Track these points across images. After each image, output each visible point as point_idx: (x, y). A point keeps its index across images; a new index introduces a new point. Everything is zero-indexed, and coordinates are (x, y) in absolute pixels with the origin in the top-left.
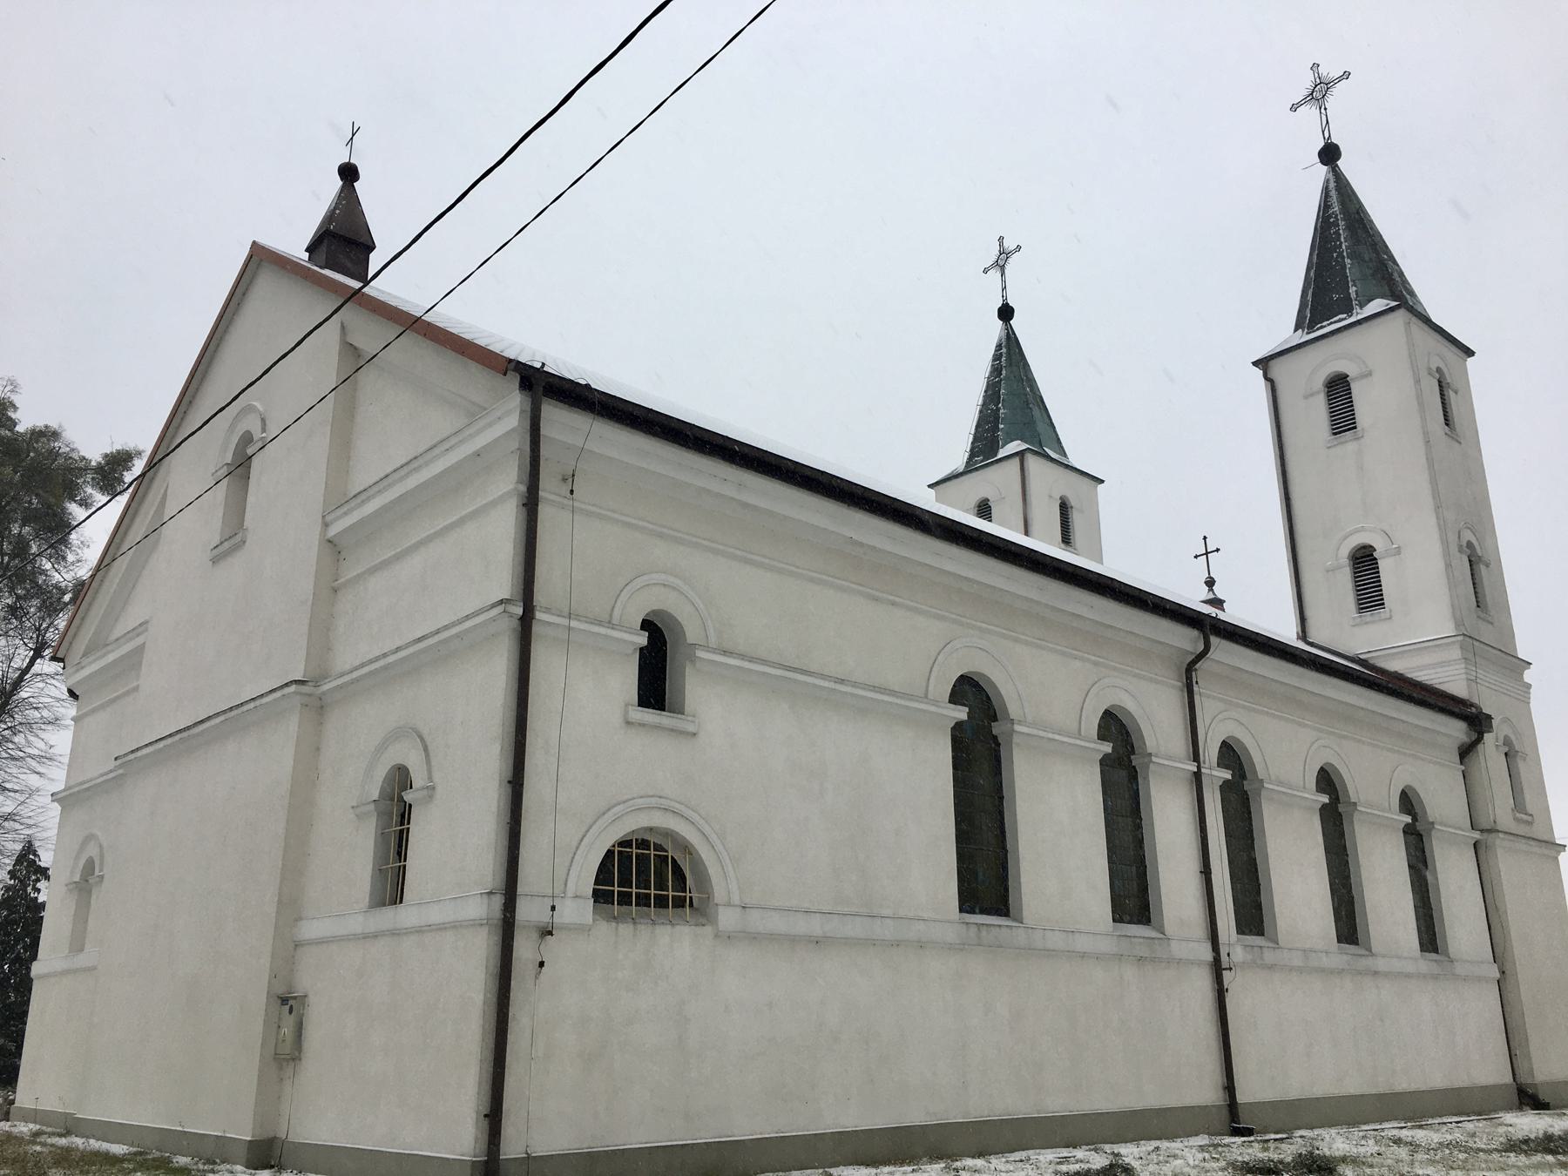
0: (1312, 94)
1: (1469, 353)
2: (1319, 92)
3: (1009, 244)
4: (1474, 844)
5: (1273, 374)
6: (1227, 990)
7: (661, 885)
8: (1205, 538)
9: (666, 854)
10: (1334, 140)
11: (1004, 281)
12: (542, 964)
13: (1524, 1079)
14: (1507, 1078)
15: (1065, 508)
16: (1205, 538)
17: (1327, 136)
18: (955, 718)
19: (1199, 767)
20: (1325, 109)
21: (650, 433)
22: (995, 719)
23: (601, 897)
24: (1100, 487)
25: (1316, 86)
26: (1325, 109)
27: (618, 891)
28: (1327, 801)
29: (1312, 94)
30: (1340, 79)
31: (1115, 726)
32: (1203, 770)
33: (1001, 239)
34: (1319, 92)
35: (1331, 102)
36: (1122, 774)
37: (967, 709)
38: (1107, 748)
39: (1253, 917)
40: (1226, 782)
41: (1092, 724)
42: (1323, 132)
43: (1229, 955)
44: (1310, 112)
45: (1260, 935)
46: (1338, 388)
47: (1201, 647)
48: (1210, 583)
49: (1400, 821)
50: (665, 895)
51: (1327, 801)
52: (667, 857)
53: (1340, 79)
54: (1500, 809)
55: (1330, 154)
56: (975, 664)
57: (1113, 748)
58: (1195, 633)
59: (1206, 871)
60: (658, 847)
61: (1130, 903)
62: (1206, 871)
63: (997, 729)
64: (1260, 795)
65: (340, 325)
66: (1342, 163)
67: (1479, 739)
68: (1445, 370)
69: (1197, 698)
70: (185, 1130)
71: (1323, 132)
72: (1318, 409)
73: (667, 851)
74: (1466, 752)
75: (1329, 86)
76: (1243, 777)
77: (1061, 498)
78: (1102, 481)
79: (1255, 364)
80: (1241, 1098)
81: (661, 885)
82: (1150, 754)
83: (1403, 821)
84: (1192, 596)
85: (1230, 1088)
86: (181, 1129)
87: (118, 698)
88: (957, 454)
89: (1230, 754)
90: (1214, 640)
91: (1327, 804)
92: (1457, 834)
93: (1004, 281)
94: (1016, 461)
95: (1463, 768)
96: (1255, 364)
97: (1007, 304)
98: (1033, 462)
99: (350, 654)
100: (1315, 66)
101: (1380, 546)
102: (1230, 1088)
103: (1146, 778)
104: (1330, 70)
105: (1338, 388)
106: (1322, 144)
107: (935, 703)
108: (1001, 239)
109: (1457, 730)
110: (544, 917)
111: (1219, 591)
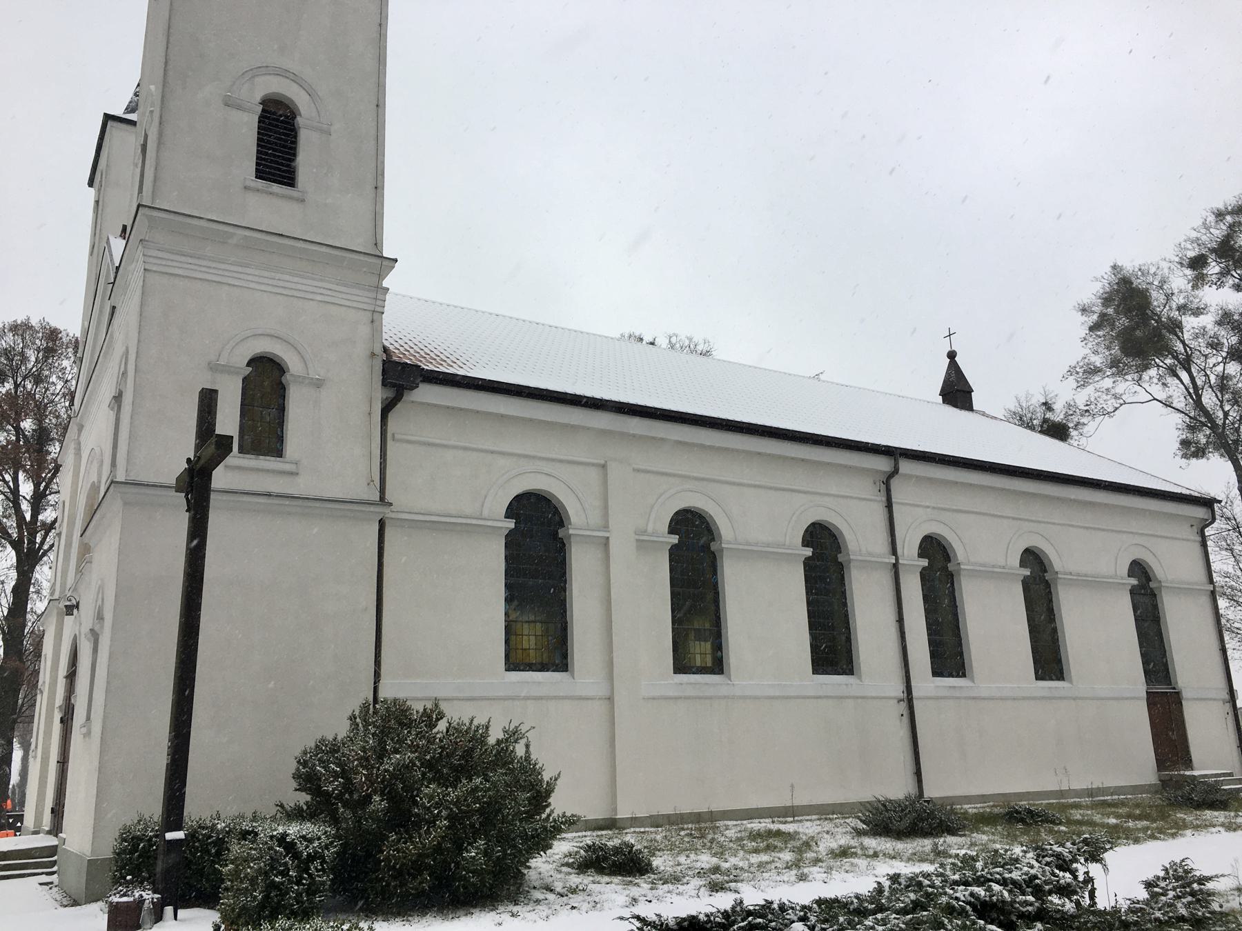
4: (380, 521)
5: (367, 313)
18: (1022, 575)
19: (897, 559)
21: (1120, 492)
22: (1046, 571)
28: (1029, 574)
37: (677, 537)
38: (1134, 581)
40: (924, 569)
41: (1124, 569)
45: (961, 677)
49: (799, 555)
50: (1166, 769)
51: (1029, 574)
55: (952, 355)
56: (1139, 554)
57: (812, 552)
63: (1048, 576)
64: (959, 575)
65: (124, 348)
76: (1149, 579)
82: (1057, 572)
83: (1129, 584)
89: (934, 548)
91: (1028, 576)
92: (1088, 580)
103: (849, 568)
107: (1122, 578)
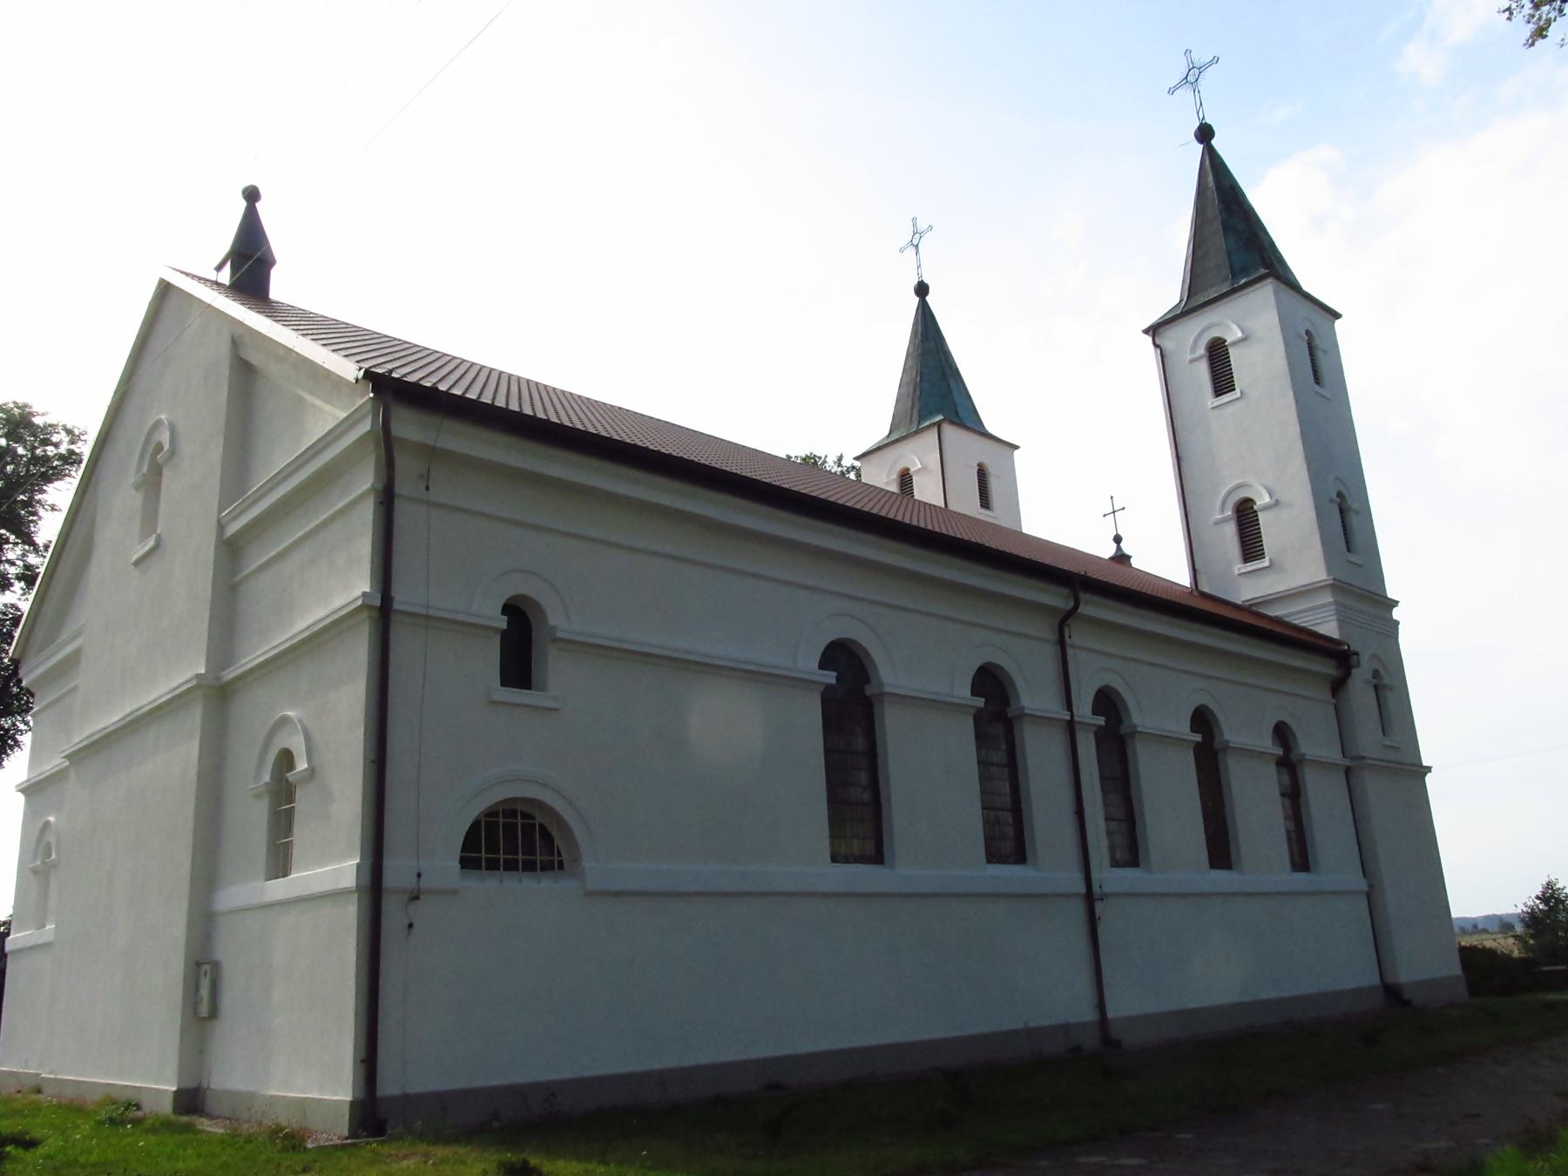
0: (1186, 78)
1: (1337, 316)
2: (1192, 77)
3: (922, 226)
6: (1099, 918)
7: (530, 850)
8: (1112, 498)
9: (533, 822)
10: (1208, 121)
11: (919, 260)
12: (411, 926)
13: (1390, 980)
14: (1376, 981)
15: (982, 474)
16: (1112, 498)
17: (1201, 118)
20: (1199, 92)
23: (468, 863)
24: (1016, 453)
25: (1190, 70)
26: (1199, 92)
27: (504, 859)
29: (1186, 78)
30: (1210, 64)
31: (990, 682)
32: (1076, 719)
33: (914, 219)
34: (1192, 77)
35: (1203, 84)
36: (999, 729)
39: (1130, 852)
42: (1198, 113)
43: (1101, 887)
44: (1185, 94)
46: (1217, 354)
47: (1072, 604)
48: (1118, 539)
52: (535, 824)
53: (1210, 64)
54: (1369, 741)
58: (1066, 591)
59: (1080, 812)
60: (525, 815)
61: (1007, 847)
62: (1080, 812)
66: (1214, 142)
67: (1348, 674)
68: (1314, 332)
69: (1070, 652)
70: (59, 1077)
71: (1198, 113)
72: (1203, 370)
73: (534, 818)
74: (1338, 686)
75: (1201, 70)
77: (979, 465)
78: (1017, 447)
79: (1146, 332)
80: (1110, 1014)
81: (530, 850)
84: (358, 653)
85: (1101, 1006)
86: (52, 1076)
87: (975, 625)
88: (878, 427)
89: (1107, 701)
90: (1083, 596)
93: (919, 260)
94: (935, 430)
95: (1334, 701)
96: (1146, 332)
97: (922, 281)
98: (950, 431)
99: (253, 655)
100: (1188, 52)
101: (1262, 499)
102: (1101, 1006)
104: (1201, 57)
105: (1217, 354)
106: (1198, 124)
108: (914, 219)
109: (1328, 668)
110: (409, 882)
111: (1126, 548)
